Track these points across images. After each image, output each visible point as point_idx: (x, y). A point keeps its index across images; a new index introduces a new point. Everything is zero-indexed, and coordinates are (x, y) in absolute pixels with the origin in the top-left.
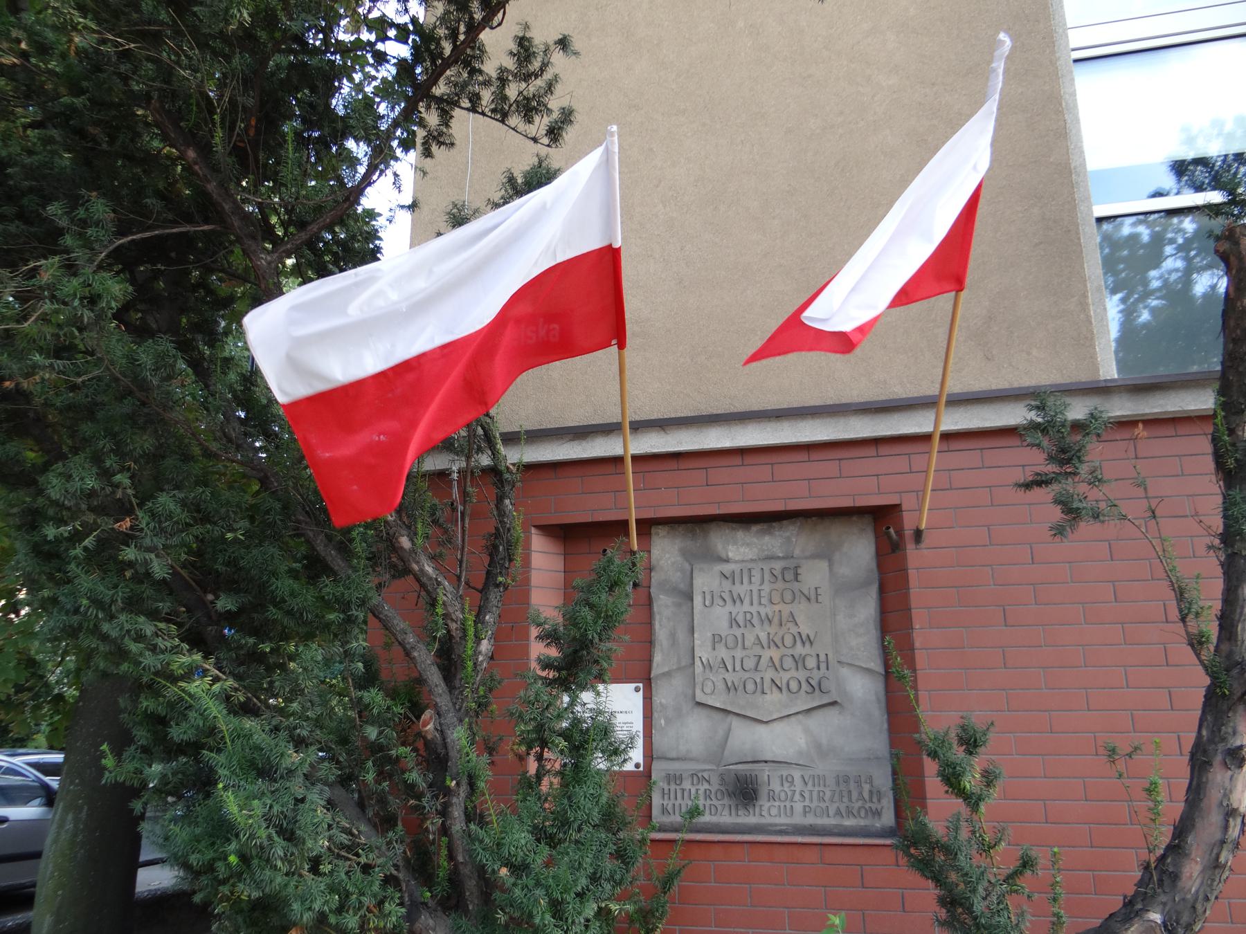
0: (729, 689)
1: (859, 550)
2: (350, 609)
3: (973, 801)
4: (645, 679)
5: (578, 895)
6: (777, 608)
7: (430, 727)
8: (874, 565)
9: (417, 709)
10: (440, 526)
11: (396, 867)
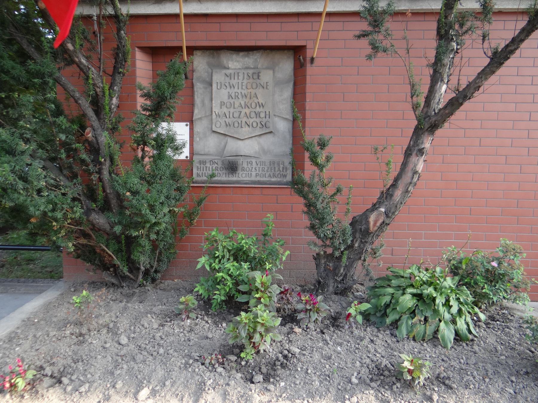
1: (286, 66)
2: (44, 77)
3: (321, 167)
4: (191, 122)
5: (161, 203)
6: (249, 91)
7: (90, 135)
8: (292, 74)
9: (83, 127)
10: (88, 41)
11: (79, 194)
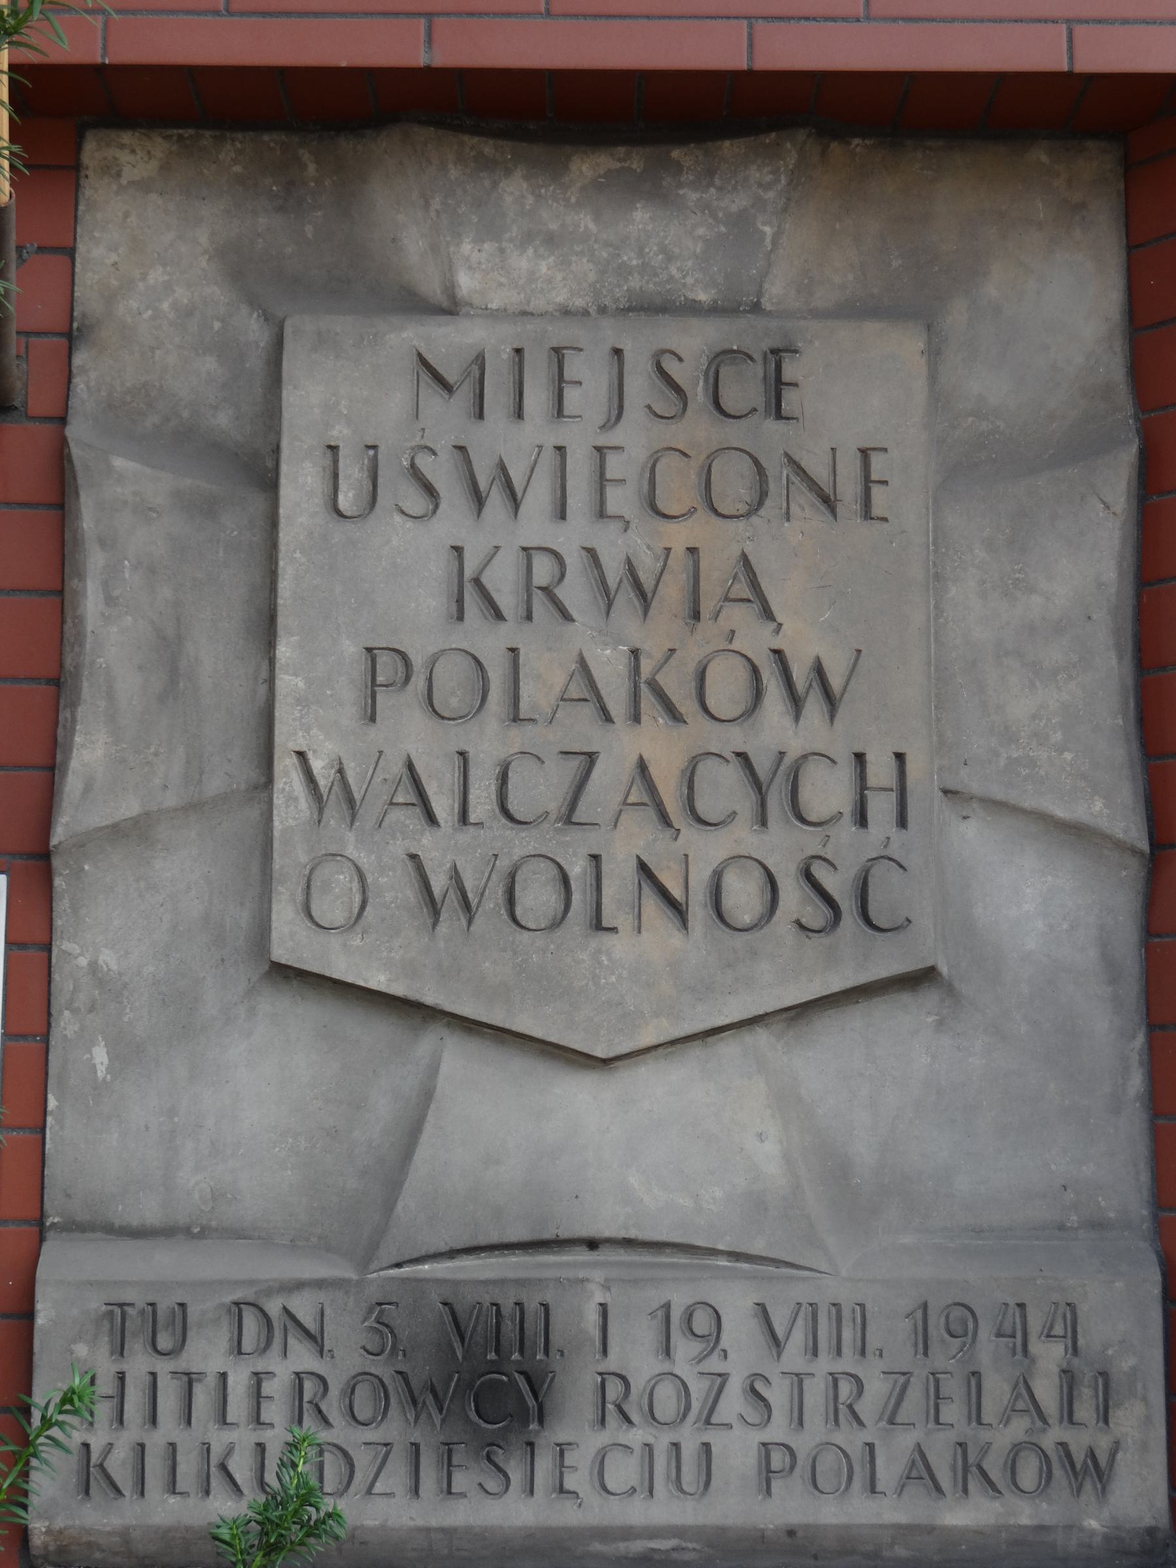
0: (433, 907)
6: (679, 536)
8: (1113, 368)
